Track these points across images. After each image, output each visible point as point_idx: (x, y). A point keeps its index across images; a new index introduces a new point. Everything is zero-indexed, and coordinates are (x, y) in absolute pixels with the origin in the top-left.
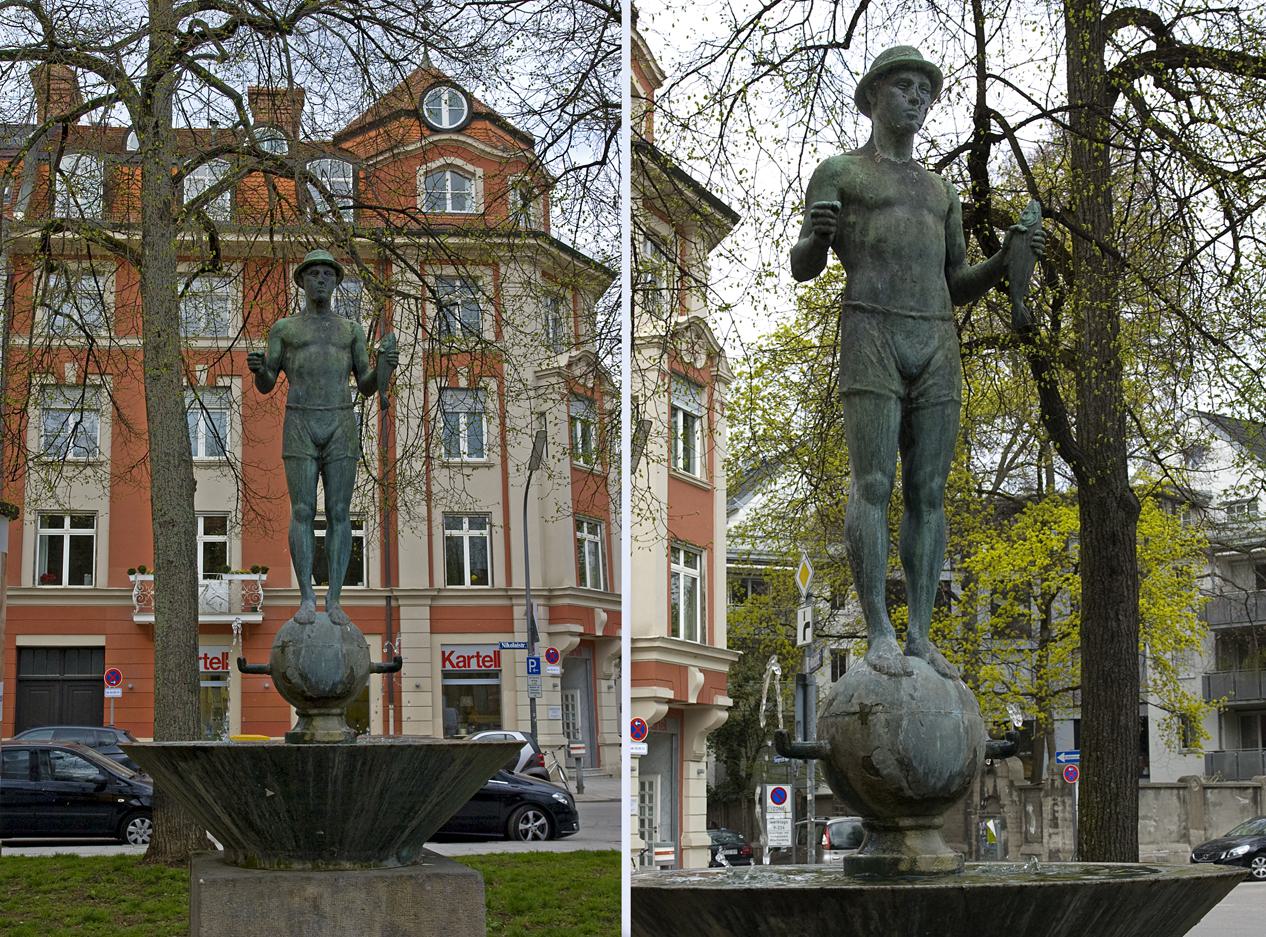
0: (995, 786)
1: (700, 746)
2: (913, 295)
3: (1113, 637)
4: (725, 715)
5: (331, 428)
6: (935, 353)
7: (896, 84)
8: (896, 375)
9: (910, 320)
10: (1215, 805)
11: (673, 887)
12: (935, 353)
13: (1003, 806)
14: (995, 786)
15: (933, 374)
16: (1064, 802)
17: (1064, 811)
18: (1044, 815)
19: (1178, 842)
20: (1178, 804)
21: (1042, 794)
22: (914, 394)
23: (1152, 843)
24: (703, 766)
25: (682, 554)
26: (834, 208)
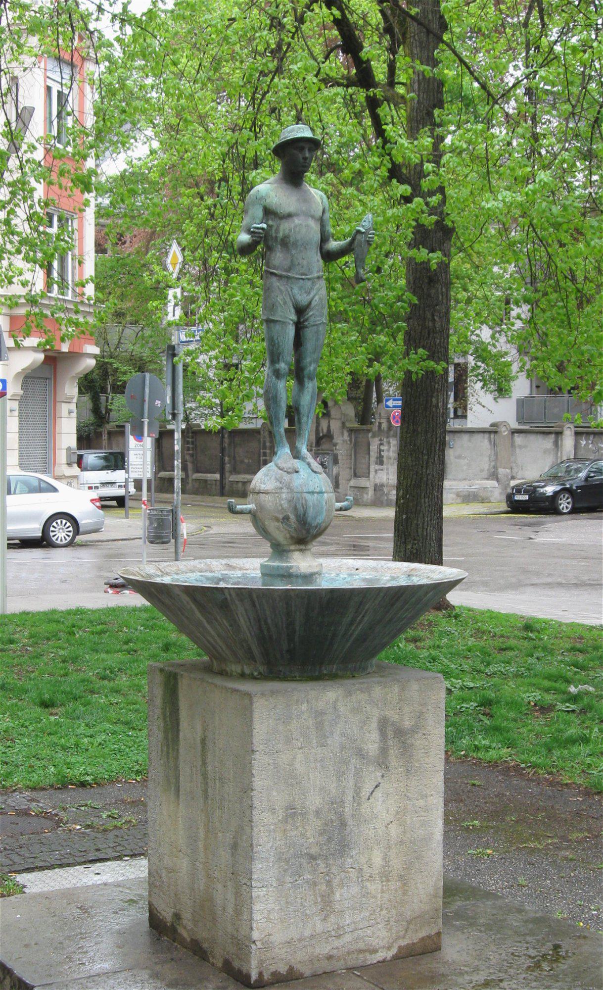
0: (329, 427)
1: (71, 390)
3: (429, 334)
4: (92, 362)
5: (311, 296)
8: (293, 310)
10: (520, 447)
11: (222, 585)
13: (335, 445)
14: (329, 427)
15: (312, 310)
16: (389, 443)
17: (388, 451)
18: (371, 453)
19: (488, 479)
20: (489, 447)
21: (370, 435)
22: (302, 320)
23: (465, 479)
24: (73, 407)
25: (55, 219)
26: (263, 229)
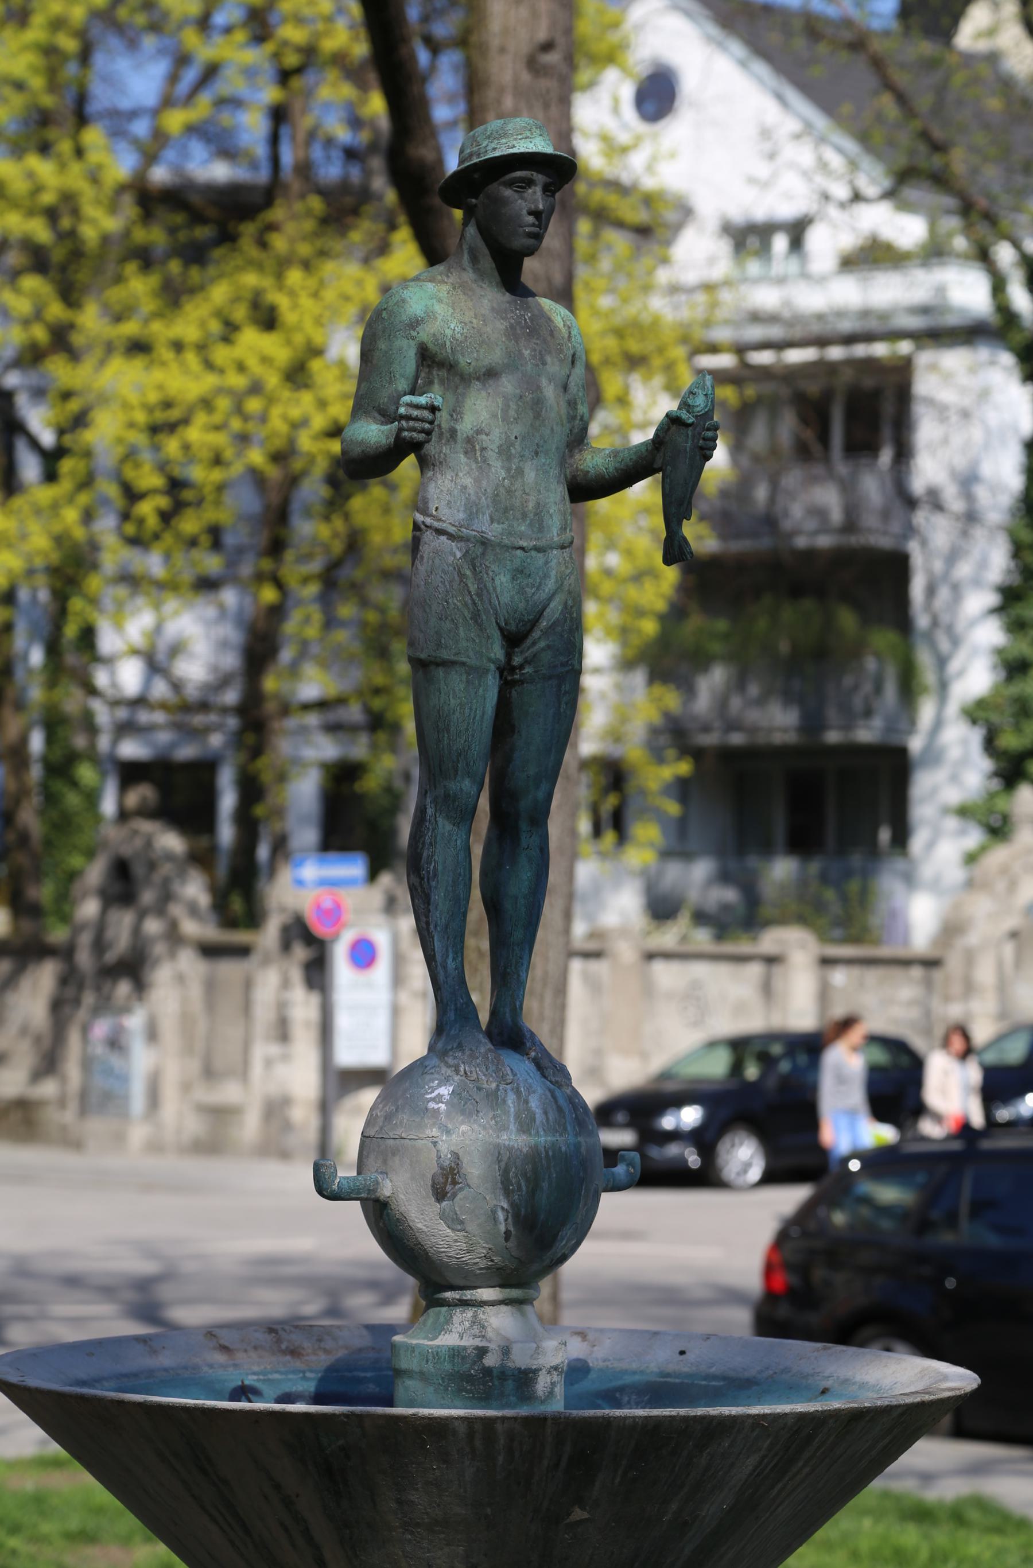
2: (524, 516)
6: (550, 599)
7: (510, 184)
9: (519, 552)
12: (550, 599)
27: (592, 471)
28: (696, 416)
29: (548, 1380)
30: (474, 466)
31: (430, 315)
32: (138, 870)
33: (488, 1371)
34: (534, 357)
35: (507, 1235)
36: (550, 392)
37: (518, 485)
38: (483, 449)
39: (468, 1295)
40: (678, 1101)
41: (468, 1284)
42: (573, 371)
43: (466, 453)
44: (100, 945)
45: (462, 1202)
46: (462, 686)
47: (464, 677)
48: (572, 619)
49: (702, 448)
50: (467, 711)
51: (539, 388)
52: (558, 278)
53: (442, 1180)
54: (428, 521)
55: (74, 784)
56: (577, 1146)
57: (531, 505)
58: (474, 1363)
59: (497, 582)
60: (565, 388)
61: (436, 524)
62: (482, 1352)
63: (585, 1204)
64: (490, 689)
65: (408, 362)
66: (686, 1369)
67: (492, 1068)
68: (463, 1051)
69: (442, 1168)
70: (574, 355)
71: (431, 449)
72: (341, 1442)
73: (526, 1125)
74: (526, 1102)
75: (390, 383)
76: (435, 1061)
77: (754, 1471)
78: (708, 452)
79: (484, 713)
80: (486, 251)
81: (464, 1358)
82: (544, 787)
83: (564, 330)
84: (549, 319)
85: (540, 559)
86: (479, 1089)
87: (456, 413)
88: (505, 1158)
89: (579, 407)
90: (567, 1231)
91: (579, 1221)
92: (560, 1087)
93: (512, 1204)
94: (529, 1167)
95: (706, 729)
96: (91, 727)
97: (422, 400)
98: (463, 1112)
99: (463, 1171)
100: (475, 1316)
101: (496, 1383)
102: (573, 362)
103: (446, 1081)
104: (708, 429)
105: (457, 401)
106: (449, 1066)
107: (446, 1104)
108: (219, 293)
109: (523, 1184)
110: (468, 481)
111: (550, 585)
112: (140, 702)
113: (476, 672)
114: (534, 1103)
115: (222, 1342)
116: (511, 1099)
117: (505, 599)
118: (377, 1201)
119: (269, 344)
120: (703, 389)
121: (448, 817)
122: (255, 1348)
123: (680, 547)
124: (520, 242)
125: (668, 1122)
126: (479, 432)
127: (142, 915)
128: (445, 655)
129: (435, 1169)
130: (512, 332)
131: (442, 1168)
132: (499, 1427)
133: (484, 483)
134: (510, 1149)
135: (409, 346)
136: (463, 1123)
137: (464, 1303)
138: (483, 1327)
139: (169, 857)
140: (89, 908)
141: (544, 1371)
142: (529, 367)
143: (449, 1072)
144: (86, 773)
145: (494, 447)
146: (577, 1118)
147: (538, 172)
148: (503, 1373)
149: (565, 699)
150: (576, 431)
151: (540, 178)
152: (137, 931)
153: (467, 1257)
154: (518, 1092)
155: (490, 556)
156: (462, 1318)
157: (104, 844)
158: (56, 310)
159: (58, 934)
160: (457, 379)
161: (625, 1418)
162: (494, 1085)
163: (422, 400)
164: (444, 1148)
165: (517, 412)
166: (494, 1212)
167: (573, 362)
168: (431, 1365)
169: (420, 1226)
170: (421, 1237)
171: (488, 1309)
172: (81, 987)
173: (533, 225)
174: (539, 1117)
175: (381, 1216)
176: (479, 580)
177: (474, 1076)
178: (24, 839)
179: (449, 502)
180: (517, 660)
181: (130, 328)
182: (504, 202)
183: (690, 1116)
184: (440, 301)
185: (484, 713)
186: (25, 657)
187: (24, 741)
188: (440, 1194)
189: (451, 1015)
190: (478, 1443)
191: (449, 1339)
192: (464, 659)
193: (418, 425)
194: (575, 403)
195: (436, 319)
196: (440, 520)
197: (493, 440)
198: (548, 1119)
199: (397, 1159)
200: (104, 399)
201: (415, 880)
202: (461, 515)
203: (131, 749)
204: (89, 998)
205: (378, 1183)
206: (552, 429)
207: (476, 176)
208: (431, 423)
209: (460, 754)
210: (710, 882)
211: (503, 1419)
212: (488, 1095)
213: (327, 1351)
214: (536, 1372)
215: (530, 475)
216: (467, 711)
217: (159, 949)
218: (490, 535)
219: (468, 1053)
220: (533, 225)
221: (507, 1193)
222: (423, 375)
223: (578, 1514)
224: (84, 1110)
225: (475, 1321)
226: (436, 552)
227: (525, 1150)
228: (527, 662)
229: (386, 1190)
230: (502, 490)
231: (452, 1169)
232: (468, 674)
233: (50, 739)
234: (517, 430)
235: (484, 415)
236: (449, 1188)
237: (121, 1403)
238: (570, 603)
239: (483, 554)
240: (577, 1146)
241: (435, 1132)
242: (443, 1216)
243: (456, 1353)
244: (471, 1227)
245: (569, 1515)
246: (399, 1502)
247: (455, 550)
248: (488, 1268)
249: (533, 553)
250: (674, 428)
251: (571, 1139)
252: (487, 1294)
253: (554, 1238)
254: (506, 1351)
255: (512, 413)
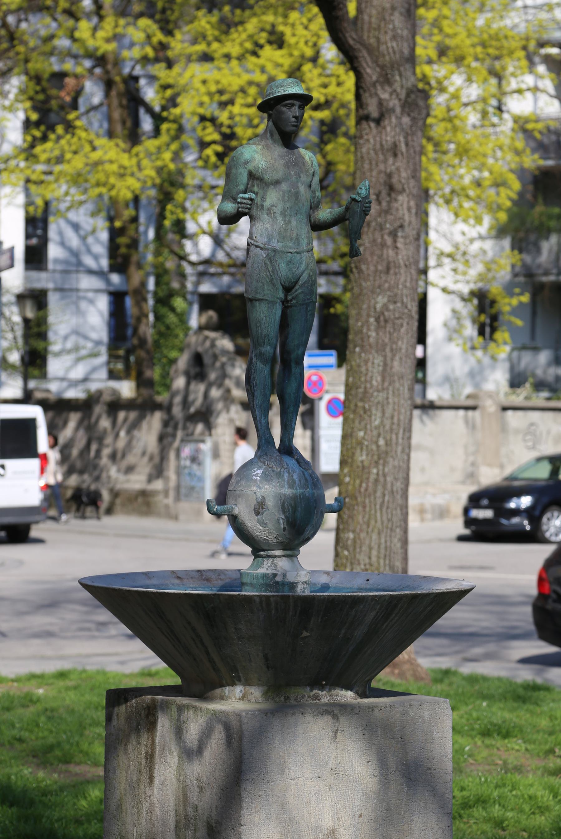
2: (291, 239)
3: (388, 269)
6: (303, 273)
7: (285, 106)
9: (289, 254)
12: (303, 273)
27: (322, 219)
28: (362, 198)
29: (302, 586)
30: (271, 220)
31: (253, 159)
32: (207, 360)
33: (277, 583)
34: (295, 175)
35: (284, 529)
36: (302, 189)
37: (289, 227)
38: (274, 213)
39: (270, 553)
40: (519, 493)
41: (270, 549)
42: (314, 179)
43: (267, 214)
44: (185, 403)
45: (265, 516)
46: (266, 309)
47: (267, 305)
48: (312, 281)
49: (364, 211)
50: (268, 319)
51: (298, 187)
52: (406, 51)
53: (258, 507)
54: (253, 242)
55: (173, 309)
56: (313, 494)
57: (294, 235)
58: (272, 580)
59: (280, 266)
60: (310, 186)
61: (255, 243)
62: (275, 575)
63: (317, 517)
64: (278, 310)
65: (243, 178)
66: (369, 587)
67: (278, 462)
68: (267, 456)
69: (258, 503)
70: (314, 172)
71: (254, 212)
72: (212, 605)
73: (292, 485)
74: (292, 476)
75: (237, 186)
76: (256, 460)
77: (375, 617)
78: (367, 212)
79: (275, 320)
80: (276, 132)
81: (268, 578)
82: (301, 349)
83: (309, 162)
84: (303, 158)
85: (298, 257)
86: (273, 471)
87: (263, 199)
88: (283, 499)
89: (317, 193)
90: (309, 528)
91: (314, 524)
92: (306, 470)
93: (286, 517)
94: (293, 502)
95: (547, 273)
96: (183, 276)
97: (247, 196)
98: (266, 480)
99: (266, 504)
100: (273, 562)
101: (281, 587)
102: (313, 175)
103: (260, 468)
104: (367, 203)
105: (264, 193)
106: (261, 462)
107: (260, 477)
108: (252, 25)
109: (290, 508)
110: (268, 226)
111: (303, 267)
112: (207, 262)
113: (271, 303)
114: (295, 477)
115: (178, 575)
116: (286, 475)
117: (284, 273)
118: (233, 515)
119: (278, 55)
120: (365, 187)
121: (261, 362)
122: (192, 578)
123: (356, 251)
124: (289, 129)
125: (512, 505)
126: (273, 206)
127: (209, 386)
128: (259, 296)
129: (255, 503)
130: (287, 165)
131: (258, 503)
132: (272, 599)
133: (275, 226)
134: (285, 495)
135: (245, 172)
136: (266, 485)
137: (269, 556)
138: (276, 566)
139: (225, 352)
140: (180, 382)
141: (300, 583)
142: (294, 178)
143: (261, 464)
144: (179, 303)
145: (279, 212)
146: (313, 482)
147: (297, 101)
148: (283, 584)
149: (309, 313)
150: (315, 202)
151: (297, 103)
152: (206, 395)
153: (268, 538)
154: (289, 473)
155: (277, 256)
156: (267, 562)
157: (189, 345)
158: (159, 36)
159: (162, 398)
160: (264, 185)
161: (321, 596)
162: (279, 470)
163: (247, 196)
164: (258, 494)
165: (288, 197)
166: (278, 520)
167: (313, 175)
168: (255, 580)
169: (249, 525)
170: (250, 530)
171: (278, 559)
172: (176, 428)
173: (295, 122)
174: (297, 482)
175: (235, 521)
176: (273, 266)
177: (271, 466)
178: (143, 342)
179: (261, 235)
180: (289, 298)
181: (201, 47)
182: (282, 113)
183: (526, 501)
184: (257, 153)
185: (275, 320)
186: (146, 232)
187: (143, 284)
188: (257, 513)
189: (263, 441)
190: (264, 605)
191: (262, 571)
192: (266, 298)
193: (245, 206)
194: (315, 191)
195: (255, 160)
196: (257, 242)
197: (278, 210)
198: (301, 483)
199: (240, 499)
200: (185, 89)
201: (249, 388)
202: (266, 240)
203: (206, 288)
204: (180, 434)
205: (233, 508)
206: (303, 204)
207: (272, 102)
208: (250, 205)
209: (265, 337)
210: (549, 365)
211: (273, 596)
212: (276, 474)
213: (221, 580)
214: (297, 583)
215: (294, 223)
216: (268, 319)
217: (220, 406)
218: (277, 248)
219: (269, 456)
220: (295, 122)
221: (284, 512)
222: (250, 183)
223: (305, 634)
224: (178, 498)
225: (273, 563)
226: (256, 255)
227: (291, 495)
228: (293, 298)
229: (236, 511)
230: (282, 229)
231: (262, 503)
232: (268, 304)
233: (157, 284)
234: (288, 205)
235: (275, 199)
236: (260, 510)
237: (129, 591)
238: (311, 274)
239: (275, 255)
240: (313, 494)
241: (255, 488)
242: (258, 521)
243: (264, 576)
244: (270, 526)
245: (302, 634)
246: (236, 629)
247: (264, 254)
248: (277, 542)
249: (295, 254)
250: (353, 202)
251: (311, 491)
252: (277, 553)
253: (304, 530)
254: (284, 575)
255: (286, 198)
